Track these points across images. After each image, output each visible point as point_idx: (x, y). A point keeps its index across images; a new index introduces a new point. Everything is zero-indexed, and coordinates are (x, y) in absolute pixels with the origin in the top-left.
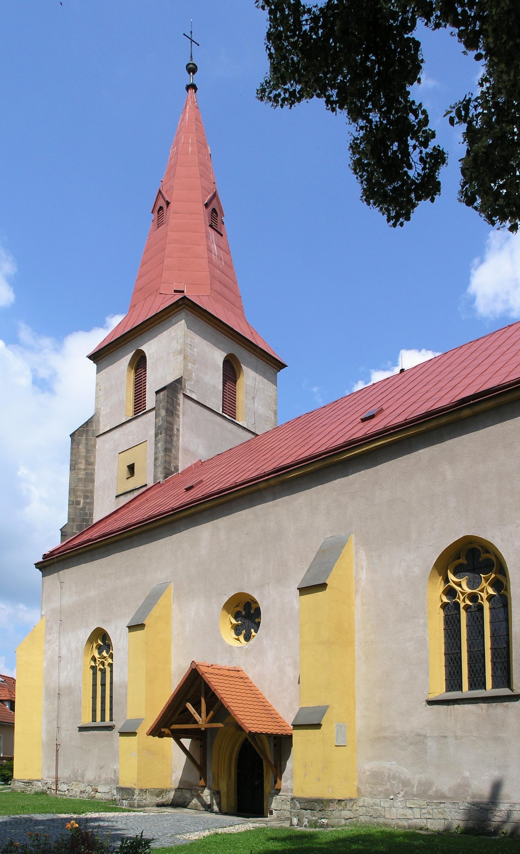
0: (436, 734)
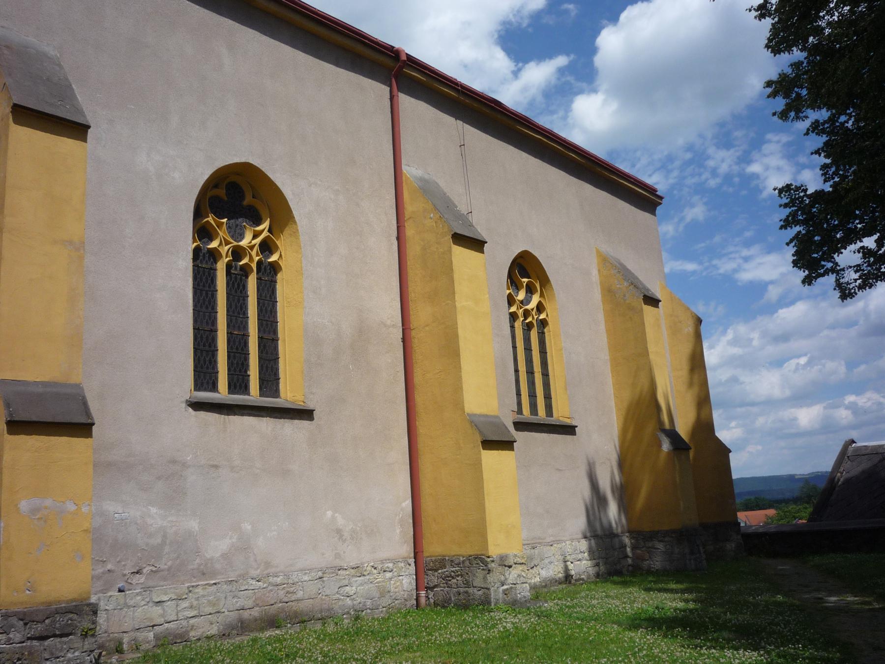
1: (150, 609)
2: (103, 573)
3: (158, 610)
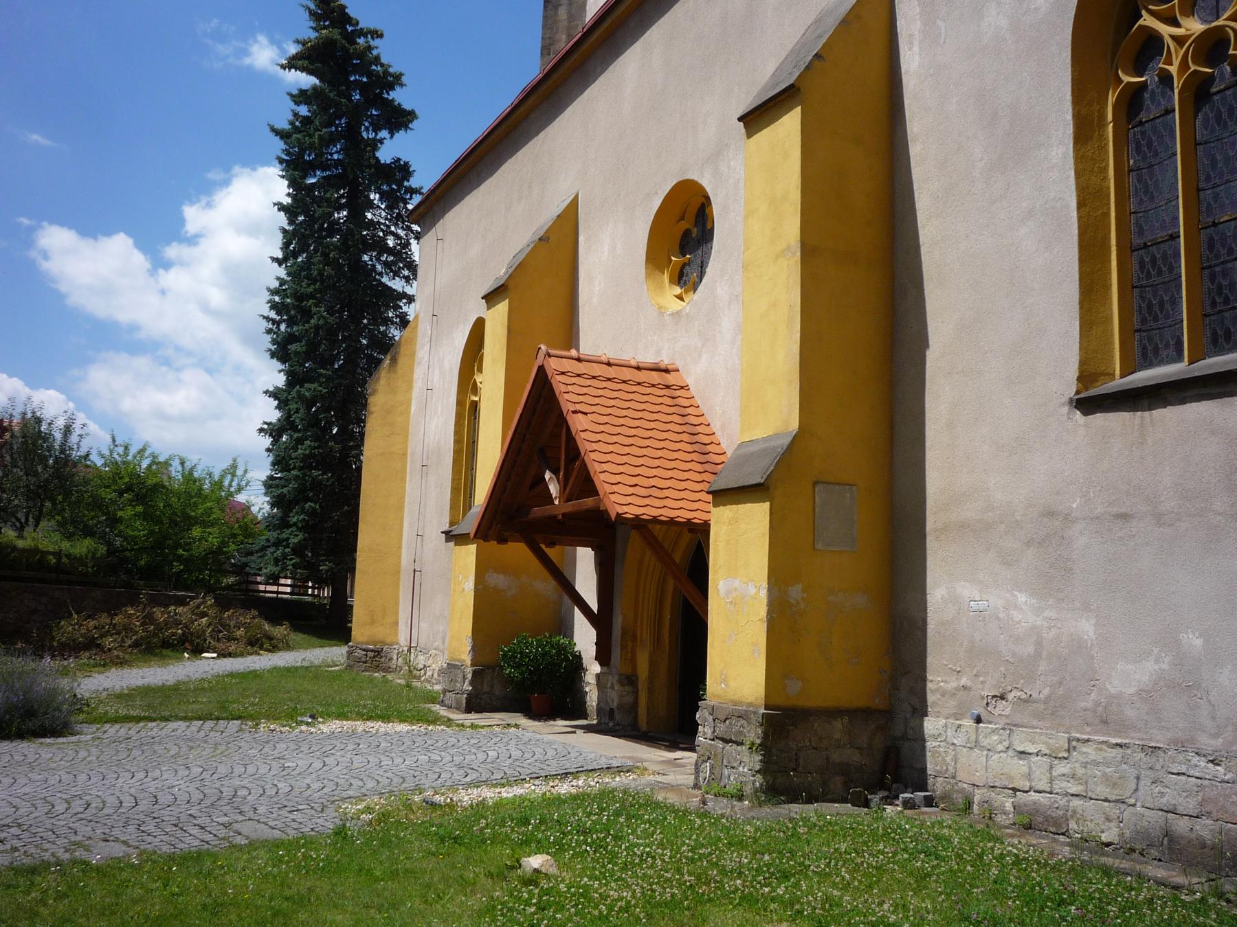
0: (1100, 510)
1: (1009, 760)
2: (957, 689)
3: (1020, 766)
